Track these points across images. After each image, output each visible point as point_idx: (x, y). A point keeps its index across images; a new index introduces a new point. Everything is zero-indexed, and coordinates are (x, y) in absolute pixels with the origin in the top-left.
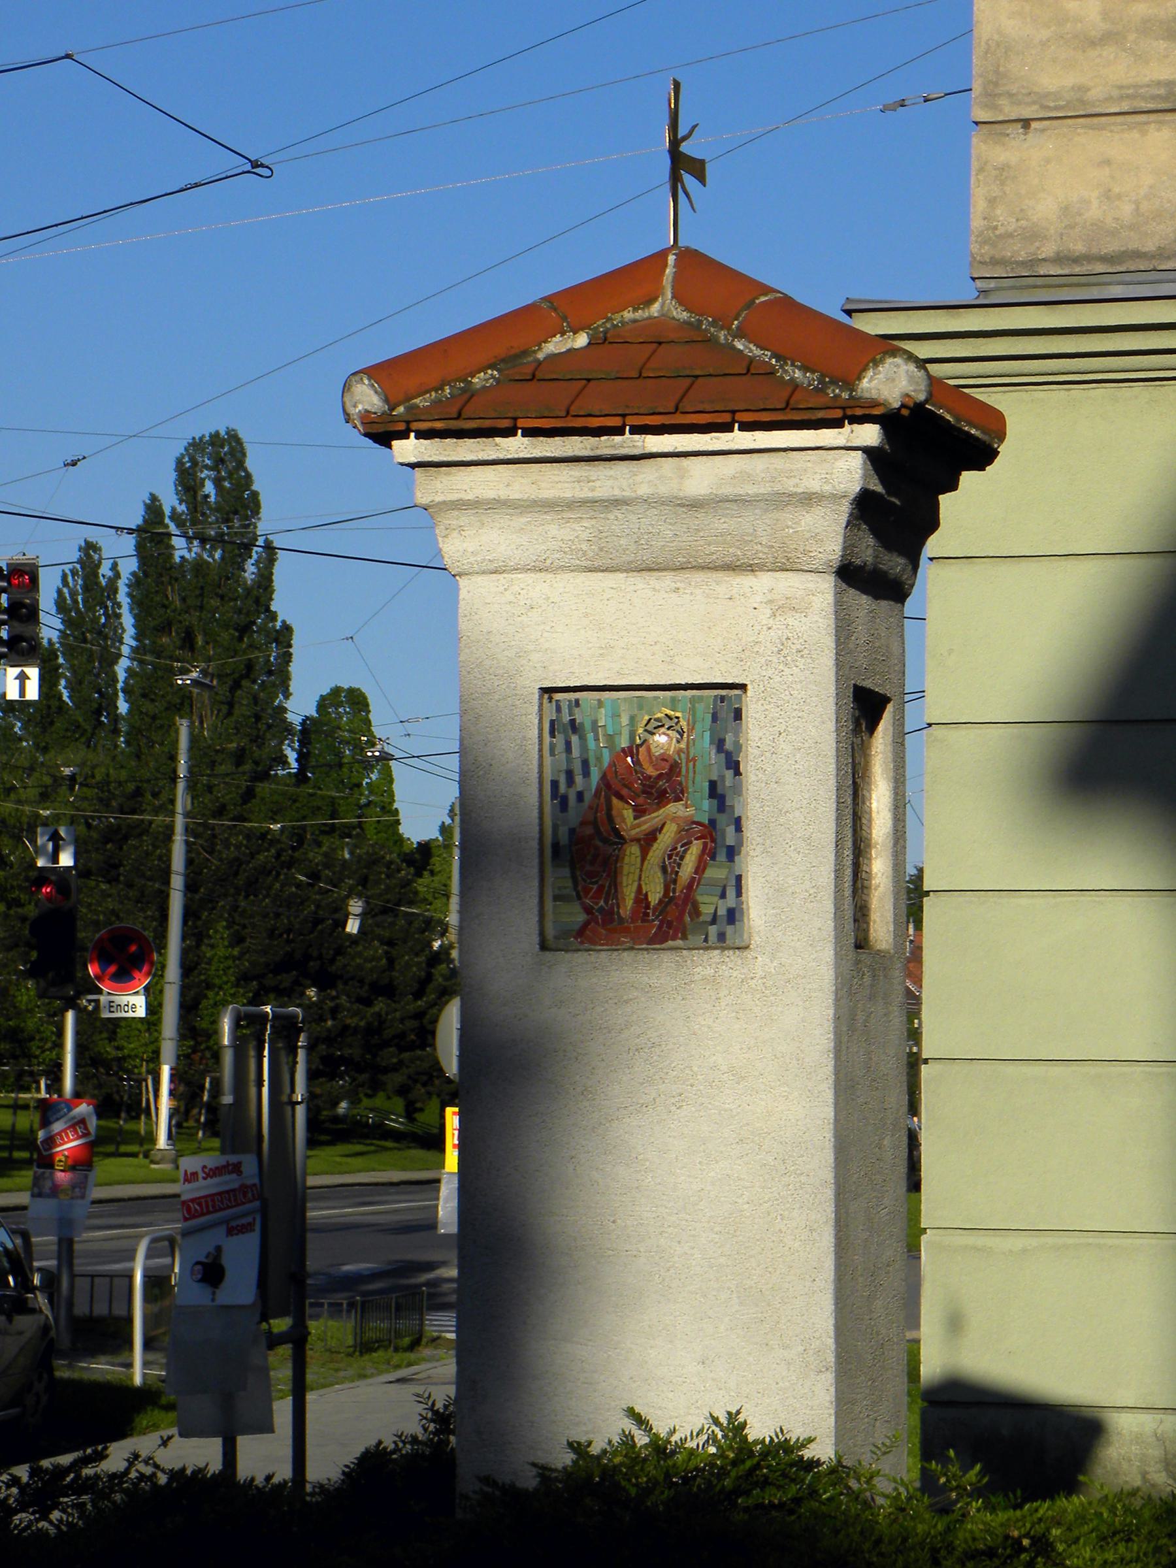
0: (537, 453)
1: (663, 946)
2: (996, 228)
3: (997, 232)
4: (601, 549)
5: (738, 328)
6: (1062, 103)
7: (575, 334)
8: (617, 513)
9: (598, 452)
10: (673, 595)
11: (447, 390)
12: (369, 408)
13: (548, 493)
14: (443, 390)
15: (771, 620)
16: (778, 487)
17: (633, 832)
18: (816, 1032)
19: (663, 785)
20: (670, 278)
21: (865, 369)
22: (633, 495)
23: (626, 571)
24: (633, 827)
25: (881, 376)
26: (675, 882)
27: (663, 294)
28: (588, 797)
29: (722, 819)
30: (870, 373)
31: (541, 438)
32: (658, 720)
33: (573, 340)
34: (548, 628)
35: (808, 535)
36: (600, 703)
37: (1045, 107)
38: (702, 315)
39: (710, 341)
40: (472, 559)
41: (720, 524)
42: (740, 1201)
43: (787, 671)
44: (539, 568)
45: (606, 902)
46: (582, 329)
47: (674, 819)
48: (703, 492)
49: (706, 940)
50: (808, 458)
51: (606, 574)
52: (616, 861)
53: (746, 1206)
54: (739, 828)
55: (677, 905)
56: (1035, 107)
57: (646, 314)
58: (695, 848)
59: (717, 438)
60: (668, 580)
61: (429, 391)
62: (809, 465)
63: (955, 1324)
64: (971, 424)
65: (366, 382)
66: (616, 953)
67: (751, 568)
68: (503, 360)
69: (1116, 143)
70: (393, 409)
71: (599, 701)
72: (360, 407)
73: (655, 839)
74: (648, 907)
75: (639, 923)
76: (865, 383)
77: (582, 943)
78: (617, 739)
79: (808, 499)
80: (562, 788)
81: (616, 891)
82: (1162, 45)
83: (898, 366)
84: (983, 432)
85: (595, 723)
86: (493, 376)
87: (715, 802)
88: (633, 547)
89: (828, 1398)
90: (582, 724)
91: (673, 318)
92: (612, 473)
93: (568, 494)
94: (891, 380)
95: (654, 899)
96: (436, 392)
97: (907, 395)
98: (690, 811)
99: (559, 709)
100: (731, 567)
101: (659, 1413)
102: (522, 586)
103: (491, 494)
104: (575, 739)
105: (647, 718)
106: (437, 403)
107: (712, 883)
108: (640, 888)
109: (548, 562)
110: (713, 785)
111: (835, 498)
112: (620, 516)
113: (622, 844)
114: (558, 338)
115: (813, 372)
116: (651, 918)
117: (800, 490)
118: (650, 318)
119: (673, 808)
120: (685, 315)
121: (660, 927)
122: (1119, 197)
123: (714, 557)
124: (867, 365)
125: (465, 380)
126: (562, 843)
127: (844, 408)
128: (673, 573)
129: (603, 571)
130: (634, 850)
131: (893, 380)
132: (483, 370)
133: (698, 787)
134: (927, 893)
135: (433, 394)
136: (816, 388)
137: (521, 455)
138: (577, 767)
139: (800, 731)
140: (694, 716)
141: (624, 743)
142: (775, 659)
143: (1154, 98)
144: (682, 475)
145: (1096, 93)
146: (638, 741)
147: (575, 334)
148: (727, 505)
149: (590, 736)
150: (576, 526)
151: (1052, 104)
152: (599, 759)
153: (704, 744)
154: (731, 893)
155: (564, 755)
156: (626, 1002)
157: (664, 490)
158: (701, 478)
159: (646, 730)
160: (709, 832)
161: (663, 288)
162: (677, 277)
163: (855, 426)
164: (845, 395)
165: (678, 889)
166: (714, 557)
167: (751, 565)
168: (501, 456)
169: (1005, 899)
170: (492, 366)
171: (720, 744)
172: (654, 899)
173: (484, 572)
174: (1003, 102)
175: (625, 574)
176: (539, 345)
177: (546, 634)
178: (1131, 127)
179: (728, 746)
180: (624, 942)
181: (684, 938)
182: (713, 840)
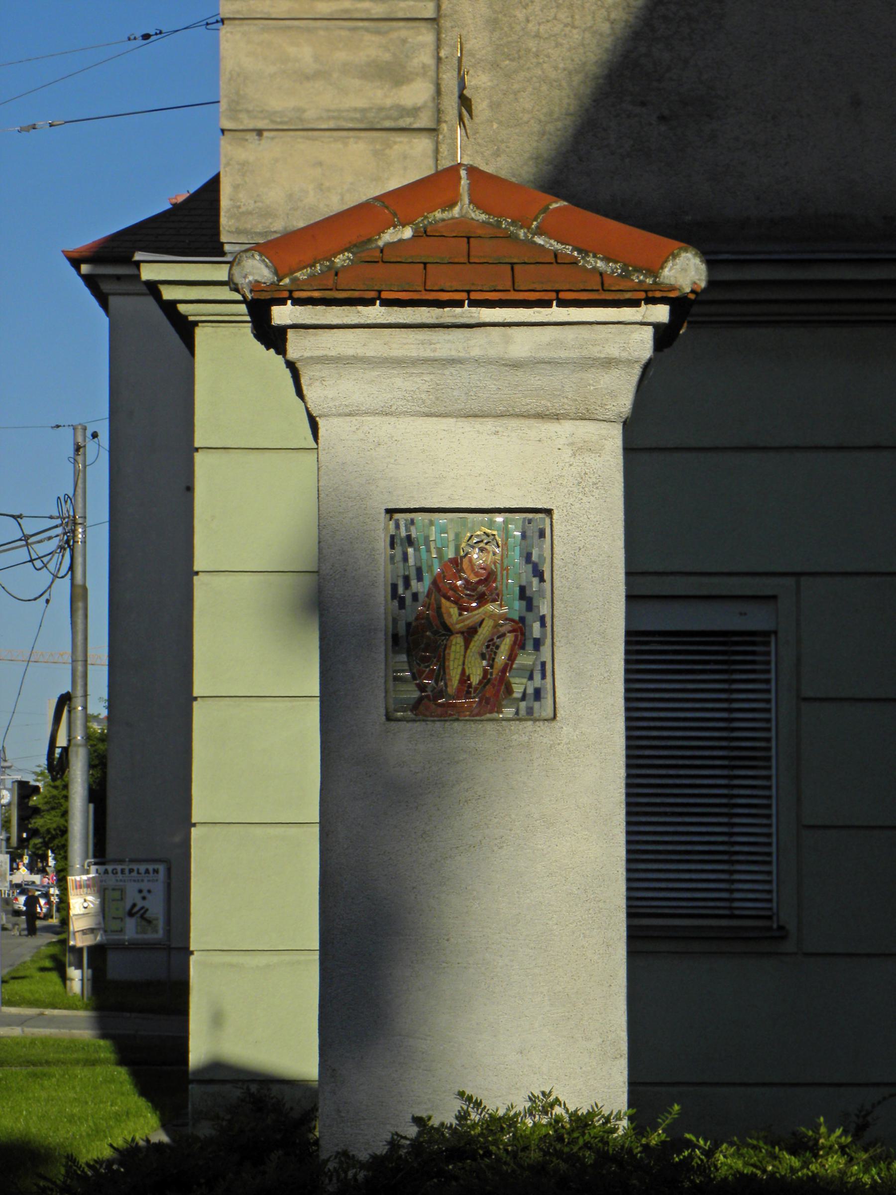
0: (392, 320)
1: (483, 718)
2: (239, 207)
3: (241, 210)
4: (437, 399)
5: (537, 227)
6: (286, 119)
8: (452, 370)
9: (442, 321)
10: (494, 437)
12: (259, 279)
15: (572, 459)
16: (585, 353)
17: (458, 626)
19: (485, 588)
20: (466, 188)
21: (666, 261)
22: (467, 356)
23: (456, 417)
25: (677, 267)
26: (492, 666)
27: (461, 200)
28: (422, 598)
29: (529, 617)
30: (670, 264)
31: (396, 308)
32: (478, 536)
33: (402, 232)
34: (392, 461)
35: (605, 392)
36: (431, 523)
37: (273, 122)
38: (501, 217)
39: (512, 238)
41: (534, 380)
42: (550, 923)
43: (585, 499)
44: (385, 413)
46: (408, 224)
48: (524, 355)
50: (610, 330)
51: (439, 419)
53: (555, 927)
54: (543, 625)
55: (494, 686)
56: (266, 121)
57: (450, 216)
58: (508, 640)
60: (489, 425)
62: (610, 336)
63: (217, 1020)
65: (258, 257)
66: (448, 723)
67: (557, 417)
68: (355, 245)
69: (326, 150)
70: (280, 280)
72: (251, 278)
74: (470, 686)
79: (608, 363)
80: (401, 590)
81: (445, 673)
82: (357, 82)
83: (689, 259)
86: (348, 258)
87: (524, 603)
91: (472, 219)
93: (414, 354)
94: (684, 270)
95: (475, 680)
97: (695, 283)
98: (505, 610)
99: (397, 526)
100: (540, 416)
101: (486, 1093)
103: (350, 352)
104: (410, 550)
105: (469, 535)
106: (312, 277)
107: (522, 668)
108: (463, 672)
109: (394, 408)
110: (522, 589)
111: (629, 362)
112: (454, 373)
113: (450, 636)
114: (391, 230)
115: (616, 262)
117: (603, 356)
118: (453, 218)
119: (490, 607)
120: (483, 217)
122: (329, 189)
123: (529, 407)
124: (668, 258)
125: (330, 260)
126: (400, 635)
127: (646, 291)
128: (493, 419)
129: (437, 416)
130: (457, 642)
132: (342, 252)
134: (196, 699)
135: (309, 269)
136: (620, 275)
137: (379, 321)
138: (413, 574)
141: (451, 555)
143: (352, 120)
144: (507, 341)
145: (310, 114)
146: (462, 554)
147: (403, 227)
148: (542, 366)
150: (418, 380)
151: (279, 120)
152: (430, 567)
153: (516, 557)
154: (537, 676)
156: (457, 762)
157: (492, 353)
158: (522, 344)
160: (520, 627)
161: (461, 195)
163: (650, 306)
164: (649, 281)
165: (495, 671)
166: (529, 407)
168: (362, 321)
169: (254, 703)
171: (528, 558)
172: (475, 680)
173: (340, 415)
174: (243, 116)
175: (455, 419)
176: (379, 235)
177: (390, 466)
178: (336, 140)
179: (534, 558)
180: (451, 715)
182: (523, 634)
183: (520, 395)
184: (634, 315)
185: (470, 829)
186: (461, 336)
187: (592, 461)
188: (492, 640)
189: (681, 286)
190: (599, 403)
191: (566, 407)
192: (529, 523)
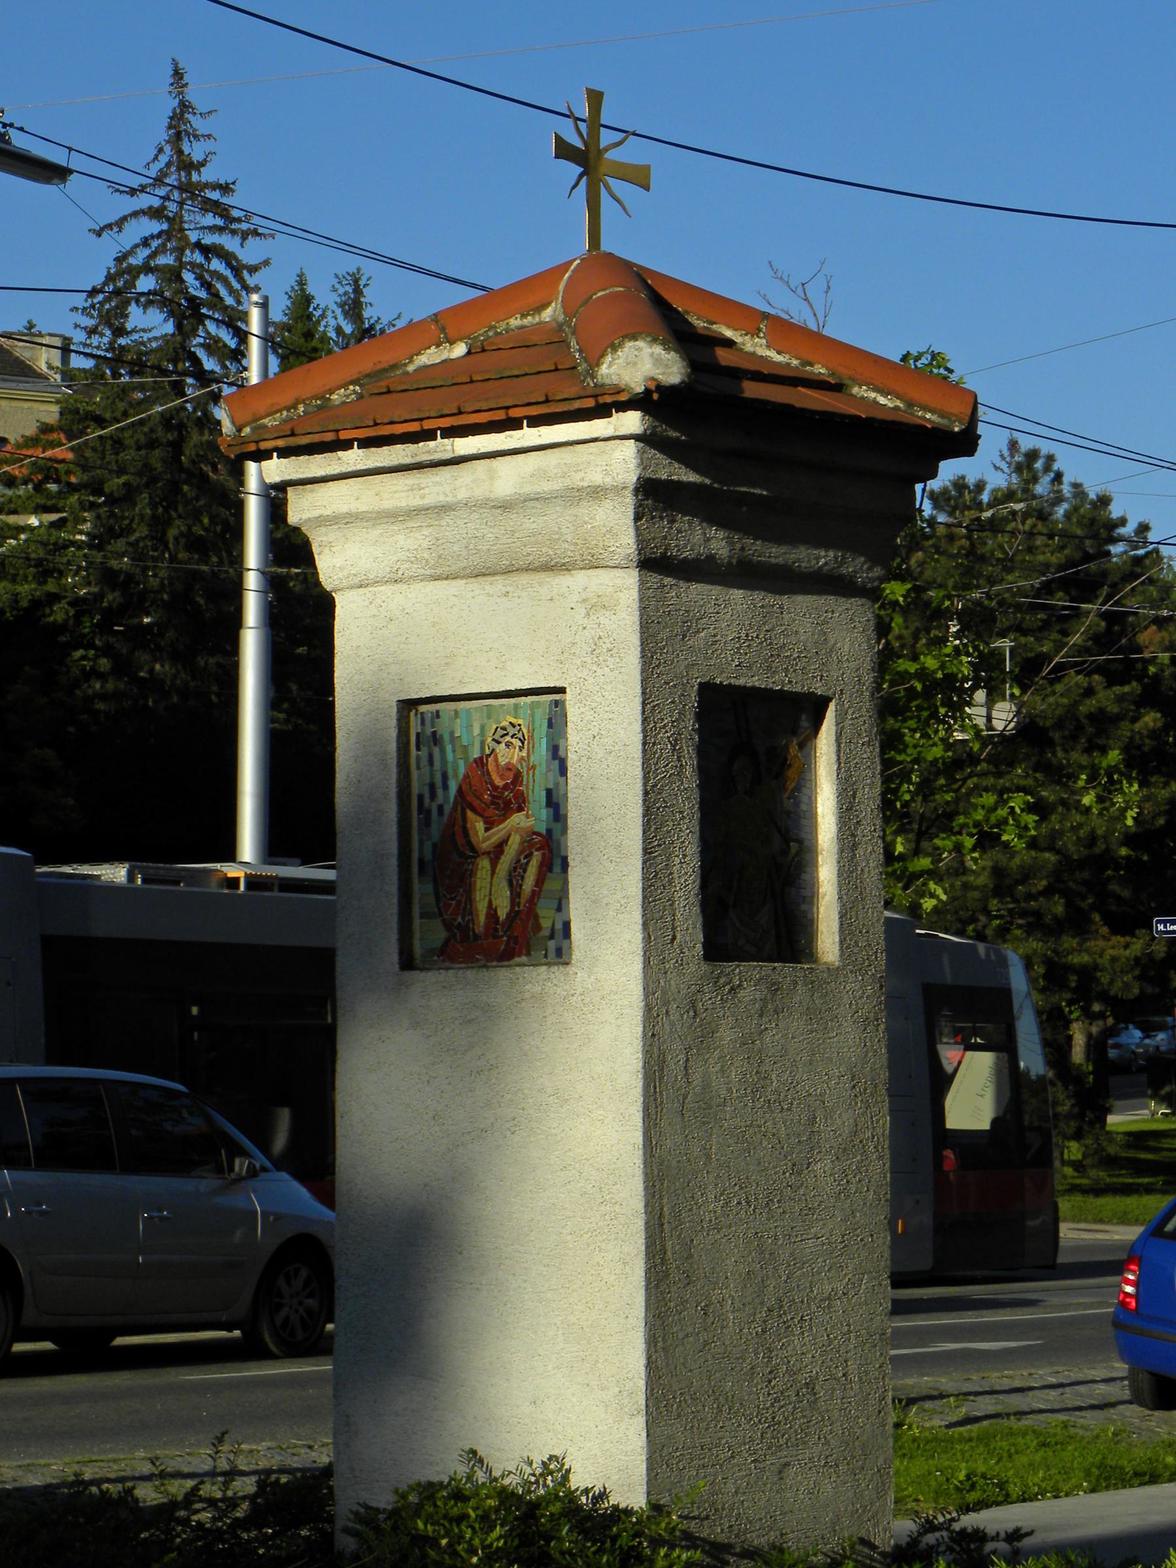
1: (511, 963)
7: (451, 344)
9: (418, 459)
10: (504, 599)
11: (301, 408)
13: (388, 504)
14: (296, 408)
15: (586, 621)
16: (568, 482)
18: (627, 1051)
19: (507, 798)
21: (603, 355)
23: (463, 577)
24: (486, 839)
25: (621, 361)
26: (519, 895)
28: (447, 809)
30: (609, 358)
32: (504, 729)
40: (340, 575)
41: (530, 523)
43: (599, 672)
45: (463, 918)
46: (461, 340)
47: (517, 830)
48: (509, 492)
49: (546, 956)
52: (471, 876)
53: (569, 1237)
58: (537, 856)
59: (511, 437)
60: (499, 584)
61: (280, 411)
62: (592, 457)
64: (925, 408)
68: (368, 376)
71: (456, 711)
73: (502, 852)
75: (491, 940)
76: (604, 369)
77: (443, 961)
78: (470, 748)
79: (596, 493)
80: (427, 801)
83: (639, 349)
84: (942, 416)
85: (452, 733)
86: (354, 392)
87: (551, 810)
88: (464, 553)
89: (640, 1444)
90: (442, 736)
92: (437, 479)
95: (502, 914)
96: (288, 410)
97: (653, 379)
98: (531, 822)
100: (549, 567)
101: (498, 1454)
102: (384, 598)
103: (344, 509)
104: (436, 751)
108: (490, 902)
110: (549, 792)
111: (618, 490)
112: (451, 522)
113: (475, 858)
116: (501, 933)
117: (585, 484)
121: (508, 942)
123: (531, 558)
125: (322, 398)
127: (596, 396)
130: (484, 863)
131: (635, 364)
132: (345, 386)
133: (536, 796)
135: (285, 413)
139: (611, 733)
140: (533, 721)
142: (589, 660)
146: (488, 752)
147: (451, 344)
148: (531, 504)
149: (449, 748)
150: (417, 535)
155: (428, 768)
157: (479, 493)
158: (507, 478)
159: (494, 740)
162: (570, 277)
165: (523, 901)
166: (531, 558)
167: (564, 564)
170: (354, 382)
172: (502, 914)
175: (464, 581)
180: (478, 960)
181: (528, 954)
182: (551, 851)
183: (518, 544)
184: (606, 428)
185: (482, 1108)
186: (449, 476)
187: (607, 622)
188: (519, 861)
189: (626, 385)
190: (601, 544)
191: (569, 553)
192: (556, 706)
